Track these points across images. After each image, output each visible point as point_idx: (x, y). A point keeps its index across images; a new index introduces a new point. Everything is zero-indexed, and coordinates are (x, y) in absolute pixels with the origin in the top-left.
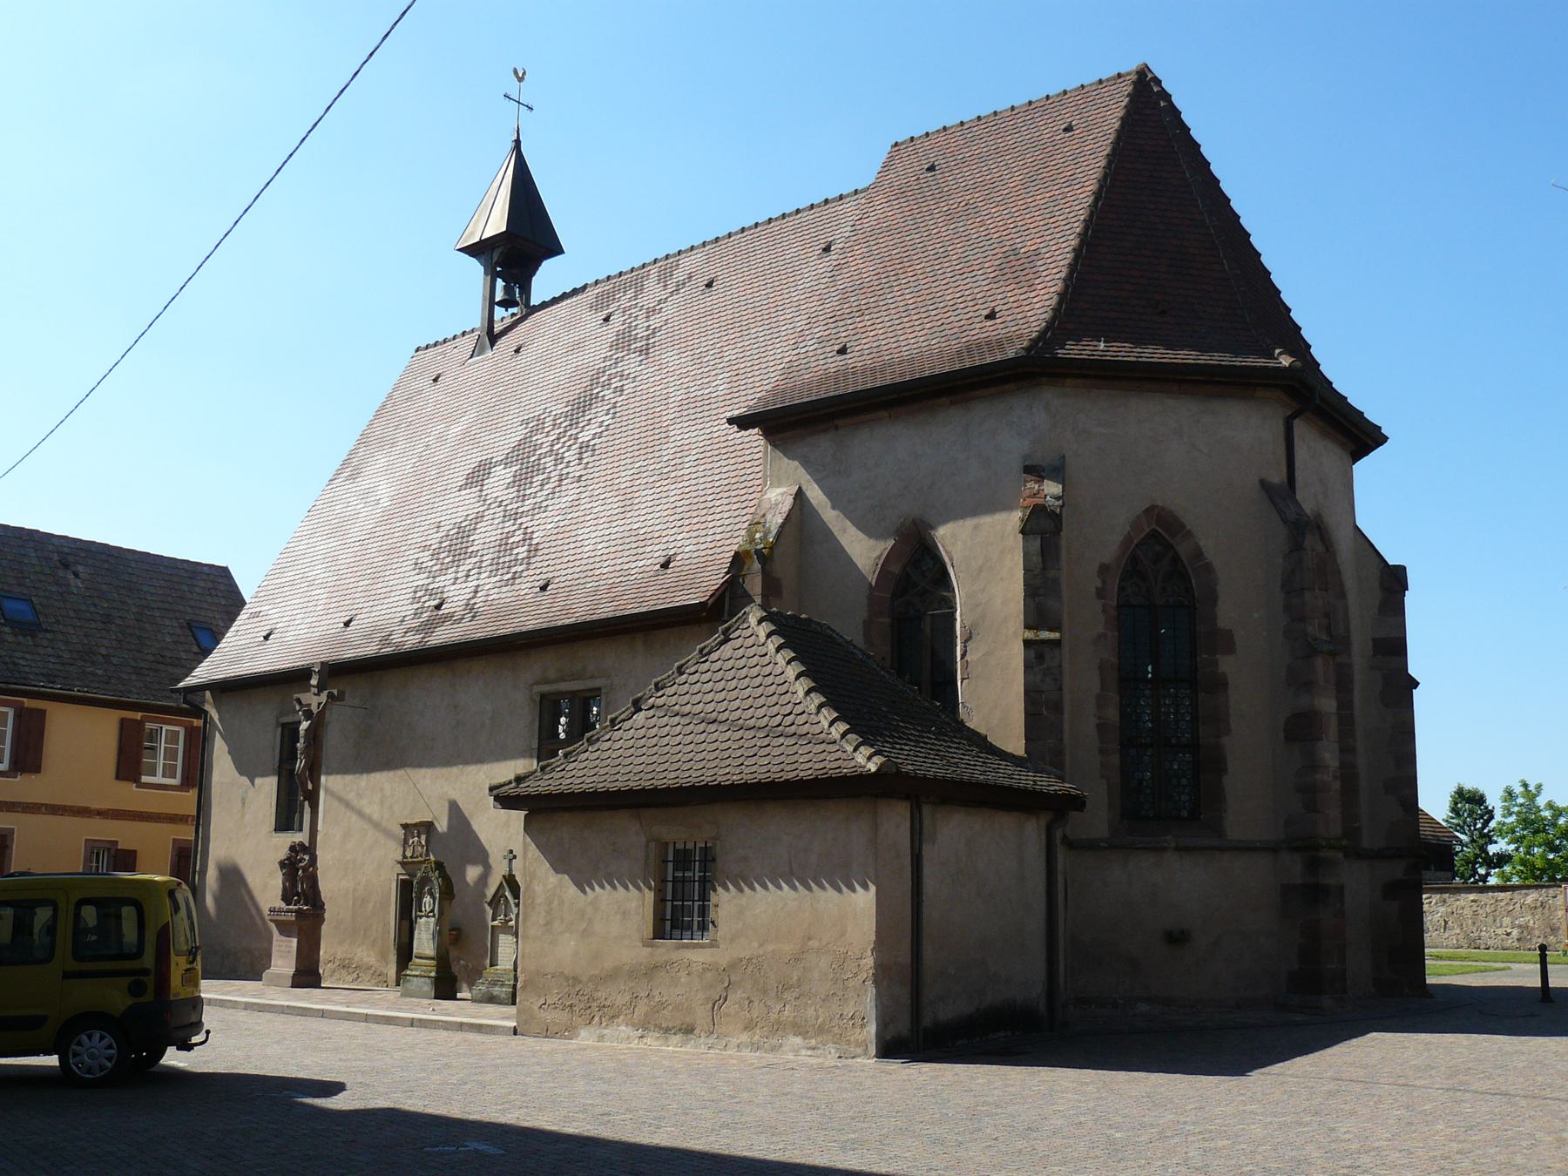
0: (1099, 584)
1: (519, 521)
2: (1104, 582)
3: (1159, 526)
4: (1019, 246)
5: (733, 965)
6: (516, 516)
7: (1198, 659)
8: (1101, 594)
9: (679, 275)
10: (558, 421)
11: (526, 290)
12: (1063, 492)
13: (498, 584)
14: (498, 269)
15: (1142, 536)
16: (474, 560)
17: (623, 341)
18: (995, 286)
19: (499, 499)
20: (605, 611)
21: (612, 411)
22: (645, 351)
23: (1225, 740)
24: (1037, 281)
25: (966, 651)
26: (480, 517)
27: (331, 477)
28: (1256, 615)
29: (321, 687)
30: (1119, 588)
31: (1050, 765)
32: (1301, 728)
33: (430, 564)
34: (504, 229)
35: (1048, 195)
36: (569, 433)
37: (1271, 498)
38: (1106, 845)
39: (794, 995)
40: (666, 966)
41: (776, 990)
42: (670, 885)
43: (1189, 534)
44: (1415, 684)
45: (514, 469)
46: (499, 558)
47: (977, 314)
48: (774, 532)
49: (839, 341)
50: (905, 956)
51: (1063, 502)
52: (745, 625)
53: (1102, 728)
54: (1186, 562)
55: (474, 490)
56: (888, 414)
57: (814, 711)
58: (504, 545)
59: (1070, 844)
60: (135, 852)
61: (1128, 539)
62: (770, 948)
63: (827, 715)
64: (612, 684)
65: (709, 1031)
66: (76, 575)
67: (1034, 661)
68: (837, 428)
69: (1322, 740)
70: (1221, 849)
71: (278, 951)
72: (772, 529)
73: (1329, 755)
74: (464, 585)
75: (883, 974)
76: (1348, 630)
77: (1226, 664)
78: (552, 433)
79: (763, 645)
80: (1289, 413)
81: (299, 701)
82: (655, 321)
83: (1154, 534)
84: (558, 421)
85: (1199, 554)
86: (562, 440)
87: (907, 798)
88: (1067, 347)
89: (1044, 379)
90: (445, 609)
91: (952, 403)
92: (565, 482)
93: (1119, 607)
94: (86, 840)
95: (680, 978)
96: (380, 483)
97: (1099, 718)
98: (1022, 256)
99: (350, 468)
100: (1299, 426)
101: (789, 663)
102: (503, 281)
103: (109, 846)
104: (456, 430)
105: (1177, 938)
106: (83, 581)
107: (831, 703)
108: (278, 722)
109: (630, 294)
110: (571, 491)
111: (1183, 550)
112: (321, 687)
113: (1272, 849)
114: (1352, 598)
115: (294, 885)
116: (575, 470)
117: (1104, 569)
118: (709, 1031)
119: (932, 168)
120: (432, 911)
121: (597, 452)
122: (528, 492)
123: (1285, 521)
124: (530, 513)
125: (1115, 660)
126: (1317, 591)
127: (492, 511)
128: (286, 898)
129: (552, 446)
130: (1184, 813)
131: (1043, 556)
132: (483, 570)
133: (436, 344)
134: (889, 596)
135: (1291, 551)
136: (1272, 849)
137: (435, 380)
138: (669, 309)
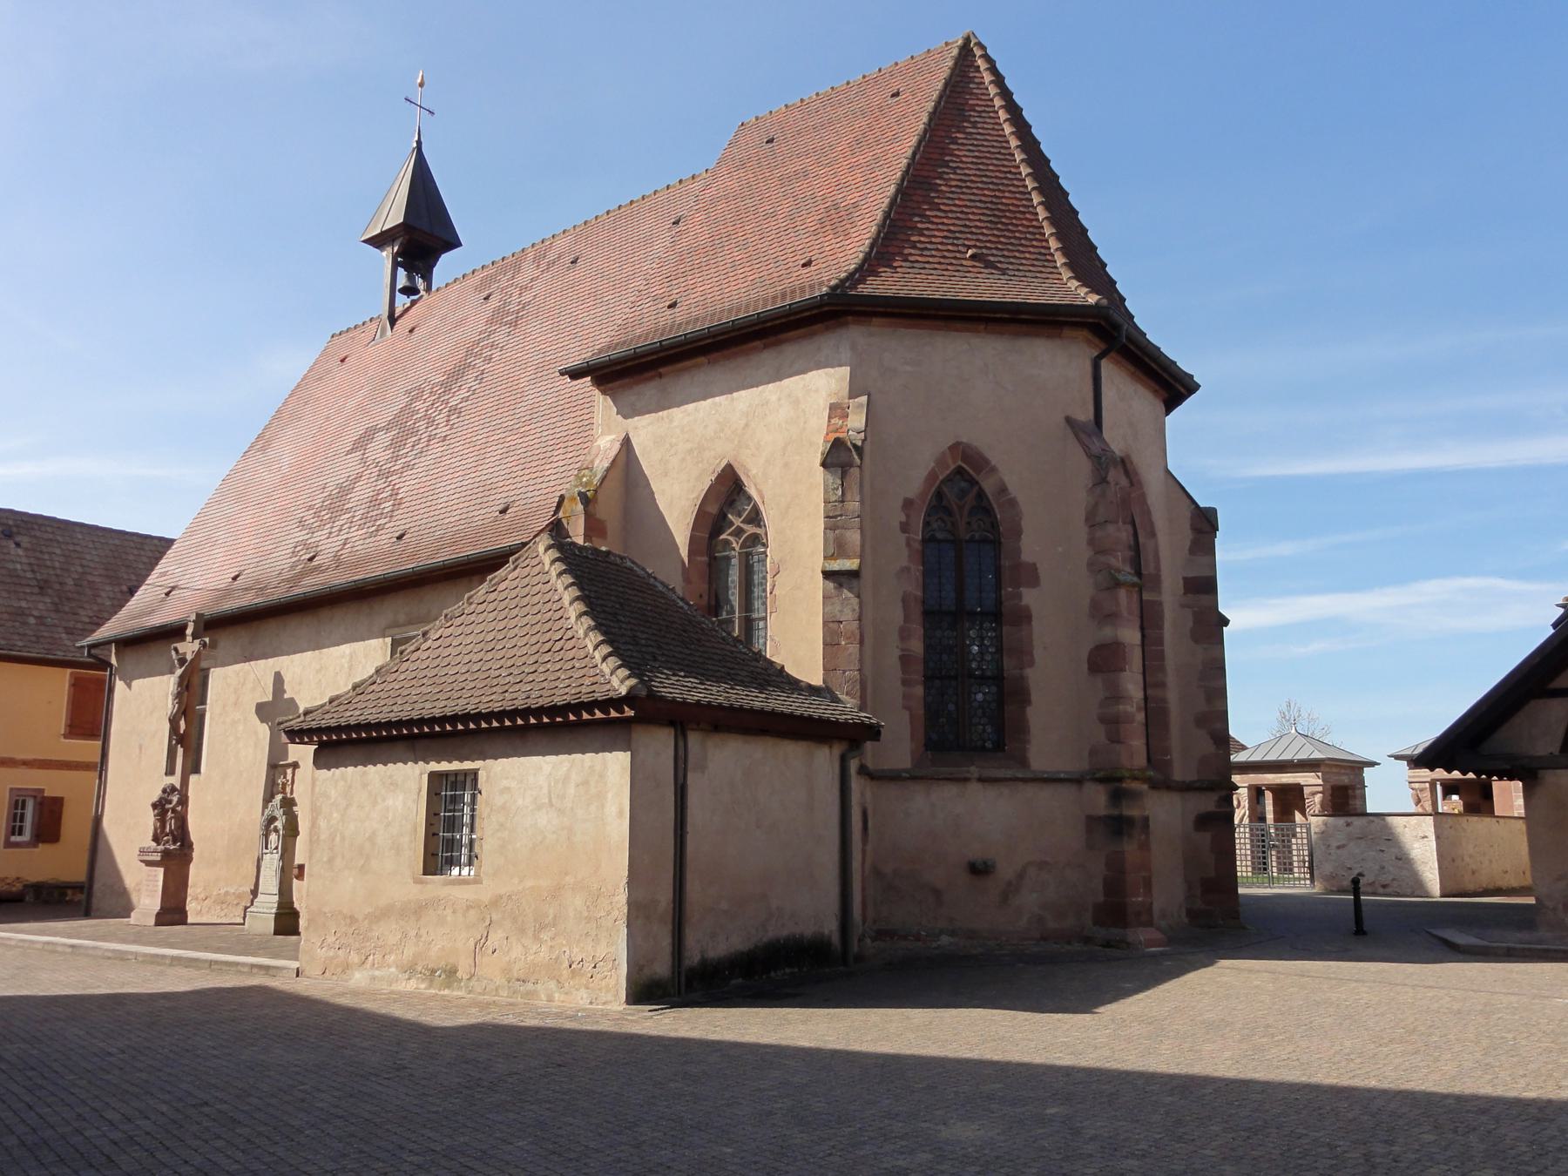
0: (903, 519)
1: (390, 479)
2: (908, 516)
3: (964, 463)
4: (840, 201)
5: (495, 902)
6: (390, 473)
7: (1003, 592)
8: (905, 527)
9: (551, 256)
10: (435, 389)
12: (866, 426)
13: (364, 536)
14: (399, 259)
15: (948, 472)
16: (347, 516)
17: (497, 318)
18: (815, 238)
19: (377, 461)
20: (445, 556)
21: (480, 377)
22: (514, 324)
23: (1029, 672)
24: (853, 230)
25: (774, 585)
26: (359, 477)
27: (246, 449)
28: (1060, 549)
29: (195, 636)
30: (923, 523)
31: (847, 694)
32: (1105, 660)
33: (312, 521)
34: (401, 220)
35: (871, 154)
36: (442, 399)
37: (1076, 436)
38: (908, 775)
39: (550, 934)
40: (434, 903)
41: (533, 929)
43: (993, 470)
44: (1226, 622)
45: (393, 433)
46: (368, 513)
47: (796, 263)
48: (599, 476)
49: (671, 298)
50: (665, 896)
51: (865, 436)
52: (535, 555)
53: (905, 659)
54: (991, 498)
55: (358, 453)
56: (707, 361)
57: (582, 636)
58: (375, 502)
59: (863, 771)
60: (62, 799)
61: (932, 476)
62: (529, 883)
63: (596, 637)
65: (470, 973)
66: (18, 545)
68: (660, 376)
69: (1125, 671)
70: (1024, 780)
71: (147, 890)
72: (598, 472)
73: (1132, 685)
74: (336, 539)
75: (638, 911)
76: (1158, 568)
77: (1029, 597)
78: (428, 400)
79: (547, 573)
80: (1096, 354)
81: (176, 650)
82: (527, 297)
83: (959, 471)
84: (435, 389)
85: (1003, 490)
86: (436, 406)
87: (671, 723)
88: (868, 282)
89: (850, 318)
91: (766, 347)
92: (432, 442)
93: (924, 541)
94: (11, 789)
95: (446, 916)
96: (286, 453)
97: (902, 650)
98: (841, 209)
99: (263, 442)
100: (1106, 365)
101: (566, 588)
102: (405, 270)
103: (34, 794)
104: (352, 403)
105: (979, 870)
106: (26, 549)
107: (598, 627)
109: (509, 275)
110: (436, 449)
111: (988, 485)
112: (195, 636)
113: (1077, 781)
114: (1163, 538)
115: (163, 826)
116: (442, 430)
117: (908, 504)
118: (470, 973)
119: (770, 141)
120: (276, 848)
121: (463, 414)
122: (401, 453)
123: (1090, 455)
124: (399, 471)
125: (919, 593)
126: (1121, 523)
127: (369, 471)
128: (156, 839)
129: (427, 411)
130: (989, 745)
132: (353, 525)
133: (348, 330)
134: (707, 536)
135: (1094, 485)
136: (1077, 781)
137: (342, 361)
138: (539, 287)
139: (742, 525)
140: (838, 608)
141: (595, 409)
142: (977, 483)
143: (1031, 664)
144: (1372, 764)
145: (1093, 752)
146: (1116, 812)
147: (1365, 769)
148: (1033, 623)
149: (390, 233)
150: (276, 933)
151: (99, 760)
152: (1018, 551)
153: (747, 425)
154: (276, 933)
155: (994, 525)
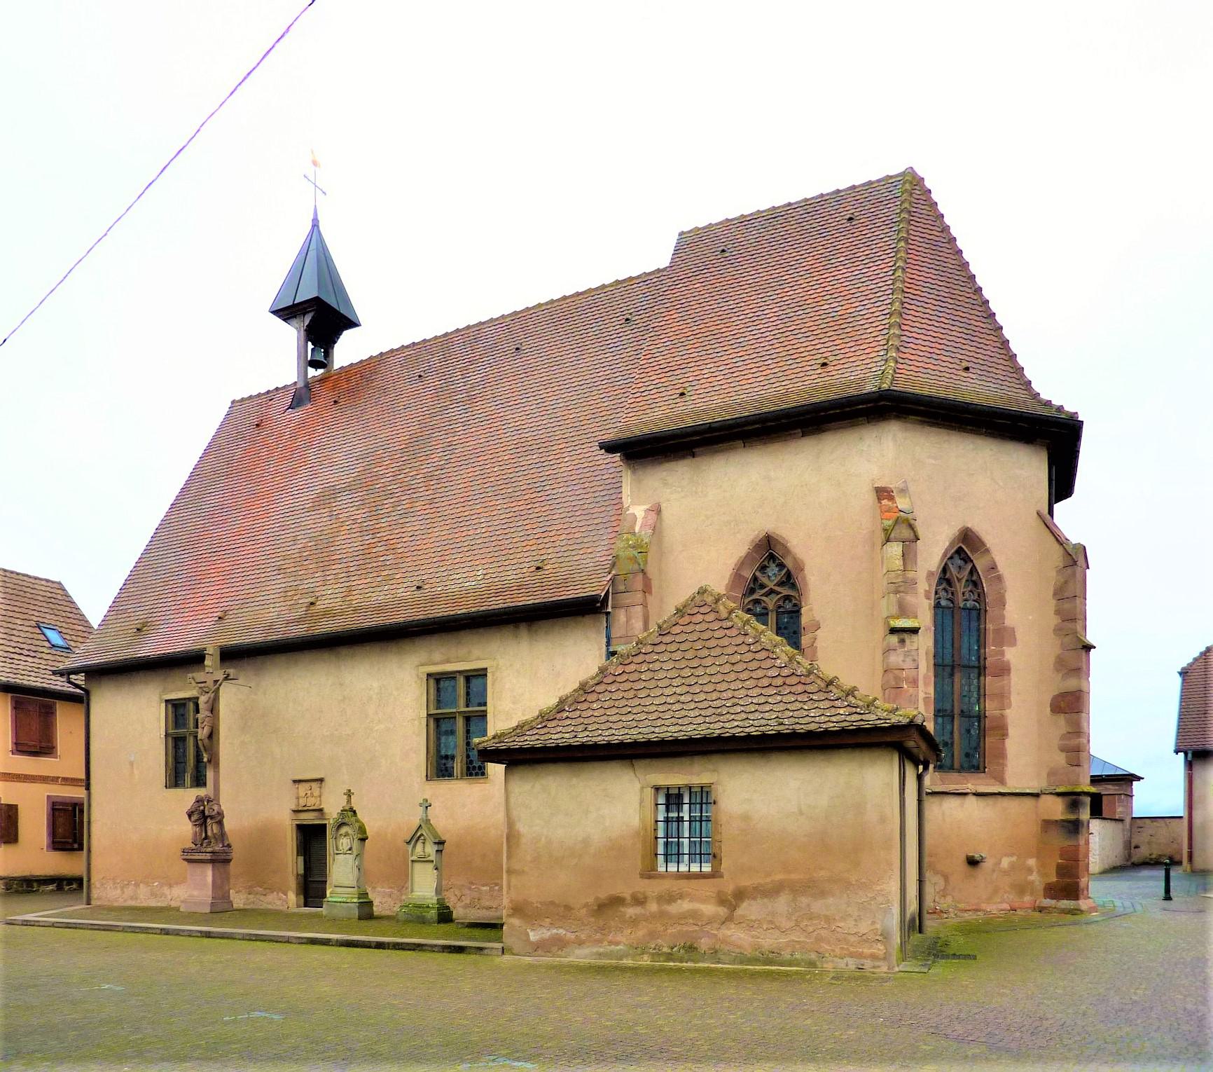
11: (328, 354)
23: (1008, 712)
28: (1030, 617)
42: (686, 824)
64: (498, 665)
67: (897, 644)
77: (1011, 655)
85: (993, 568)
90: (320, 606)
108: (161, 700)
131: (904, 560)
139: (773, 588)
140: (901, 658)
141: (624, 484)
142: (972, 561)
143: (1010, 706)
144: (1139, 779)
145: (1052, 773)
146: (1072, 817)
147: (1134, 783)
148: (1011, 674)
149: (300, 307)
150: (360, 918)
151: (1013, 785)
152: (1003, 617)
153: (785, 502)
154: (360, 918)
155: (981, 597)
